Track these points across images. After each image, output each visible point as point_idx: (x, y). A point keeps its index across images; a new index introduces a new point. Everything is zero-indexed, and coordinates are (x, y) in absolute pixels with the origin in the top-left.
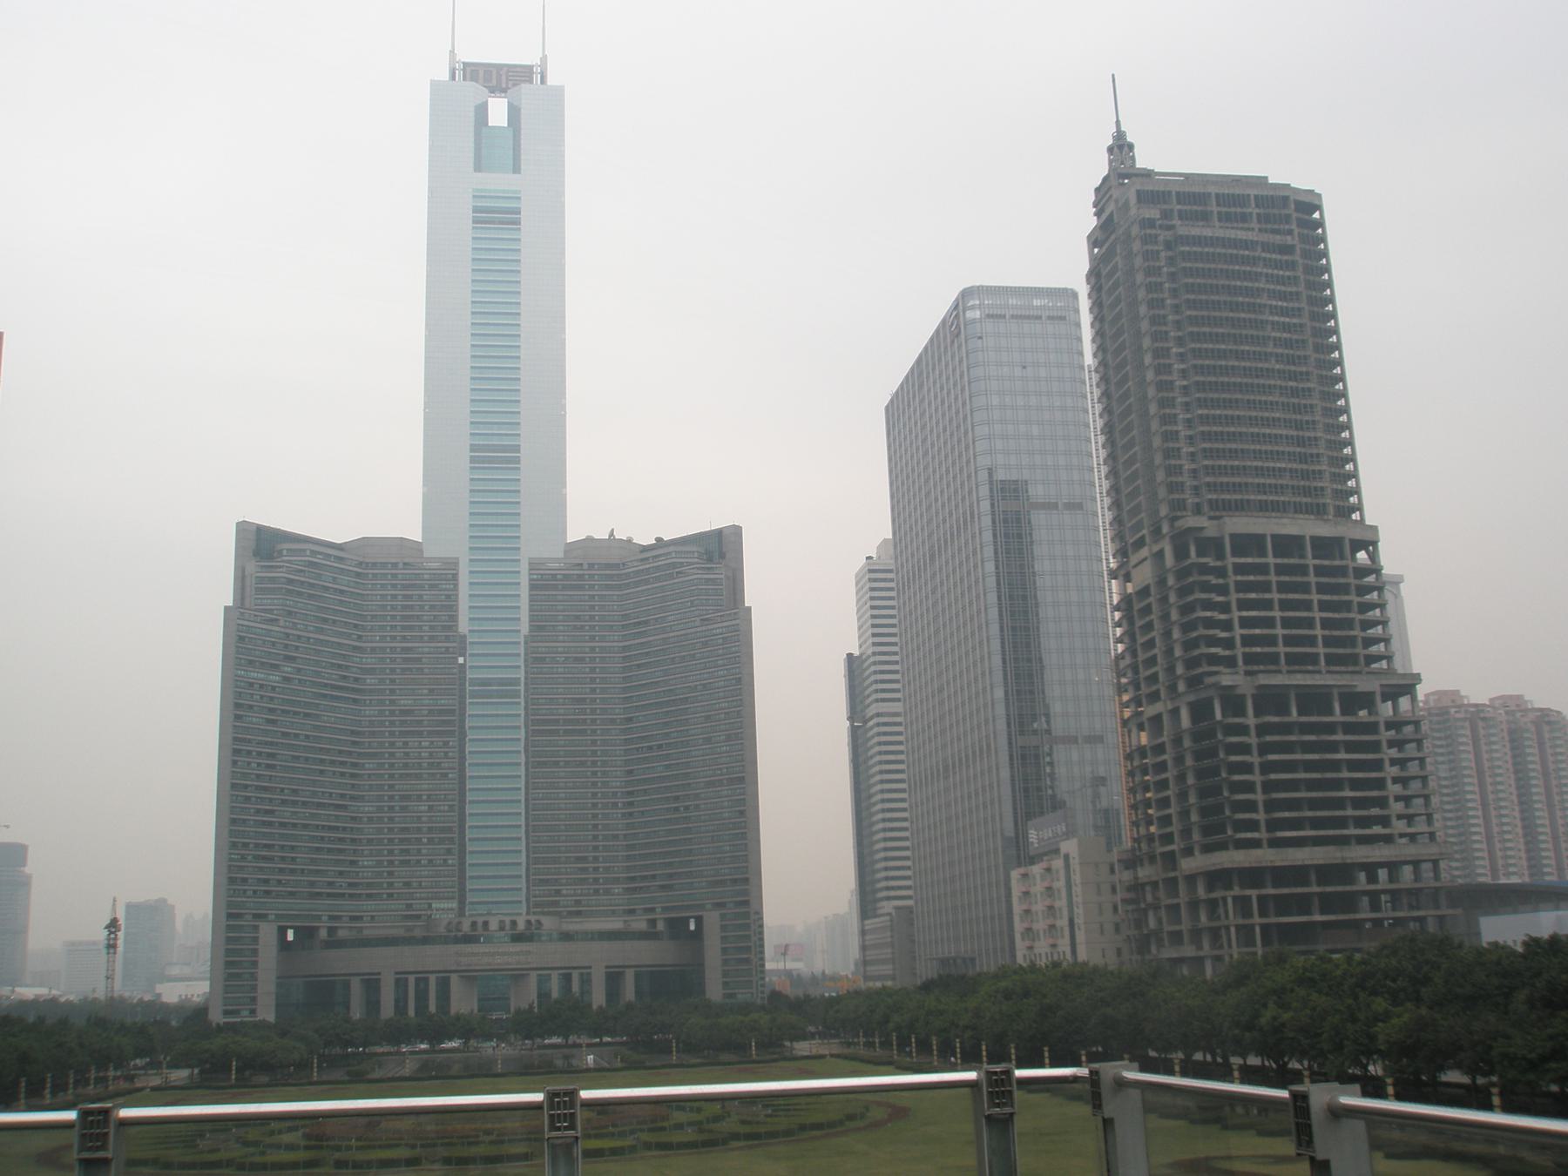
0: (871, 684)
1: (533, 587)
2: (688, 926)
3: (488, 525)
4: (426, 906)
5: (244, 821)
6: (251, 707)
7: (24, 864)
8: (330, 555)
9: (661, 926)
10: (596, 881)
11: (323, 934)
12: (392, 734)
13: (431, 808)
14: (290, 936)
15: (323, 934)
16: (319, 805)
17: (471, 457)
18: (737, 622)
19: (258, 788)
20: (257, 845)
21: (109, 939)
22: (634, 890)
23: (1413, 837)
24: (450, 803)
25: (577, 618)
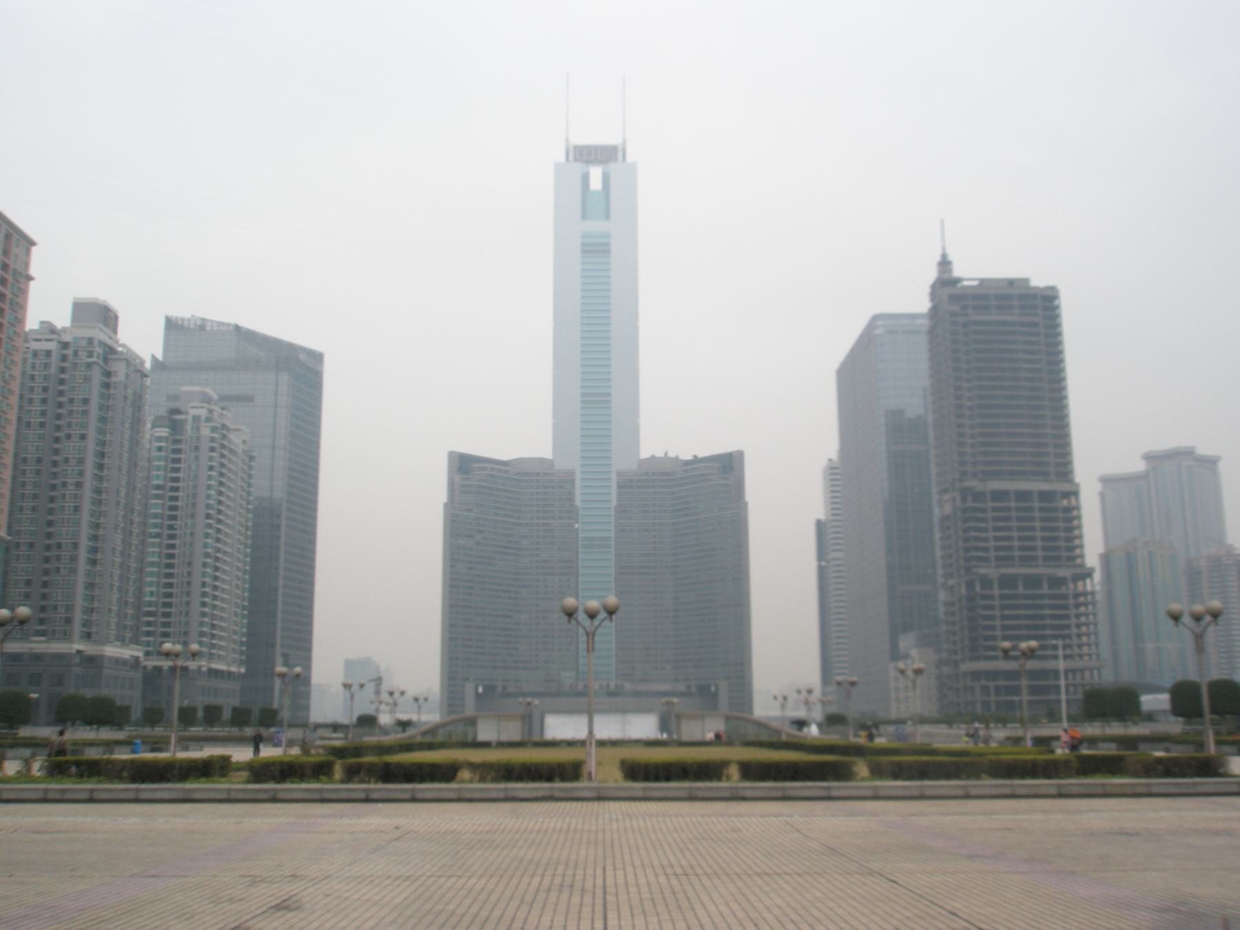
1: (620, 487)
9: (694, 689)
14: (480, 689)
15: (499, 689)
23: (1081, 656)
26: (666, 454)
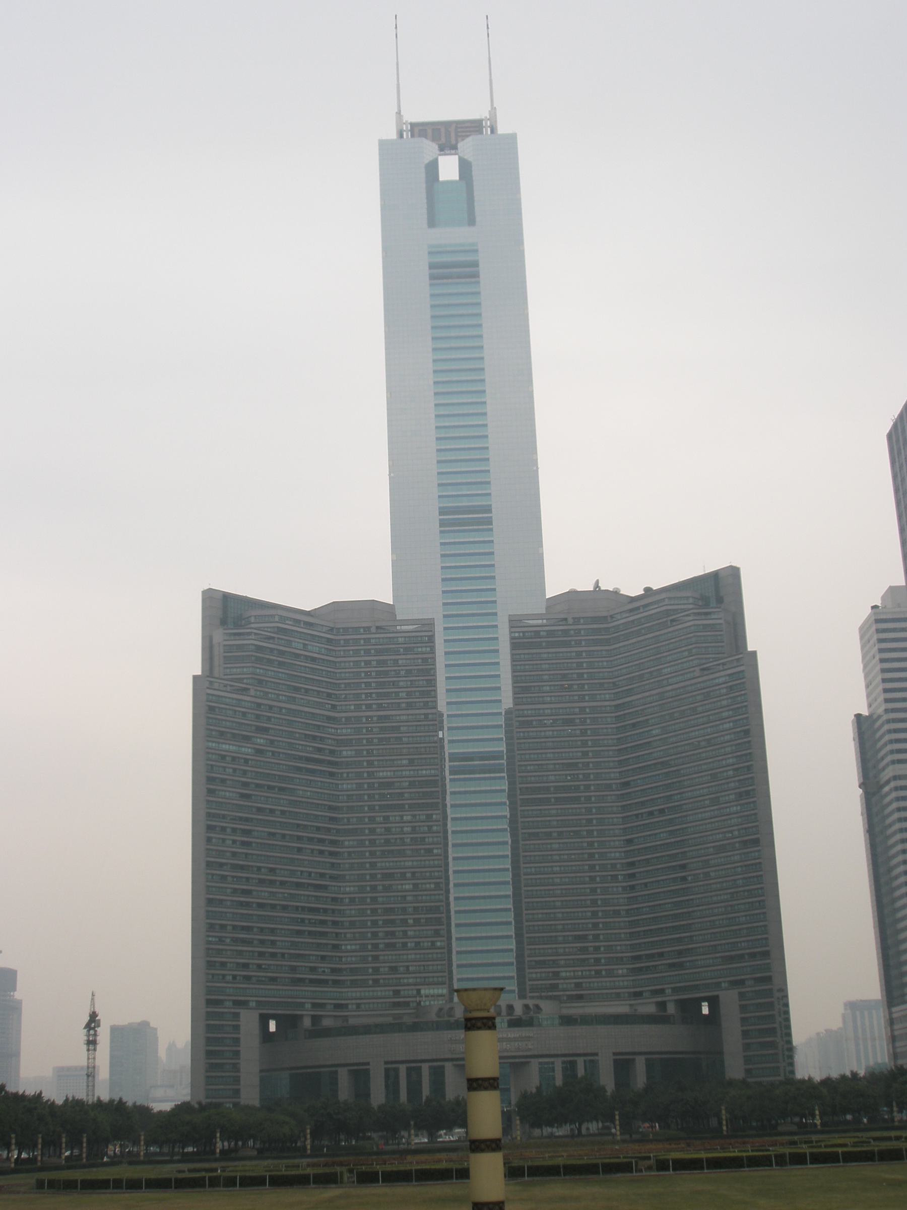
0: (885, 745)
4: (415, 992)
5: (221, 901)
6: (223, 781)
8: (300, 621)
9: (671, 1009)
11: (307, 1023)
12: (372, 809)
13: (415, 886)
14: (272, 1026)
15: (307, 1023)
16: (298, 885)
18: (742, 668)
19: (235, 867)
20: (234, 927)
21: (88, 1035)
25: (564, 677)
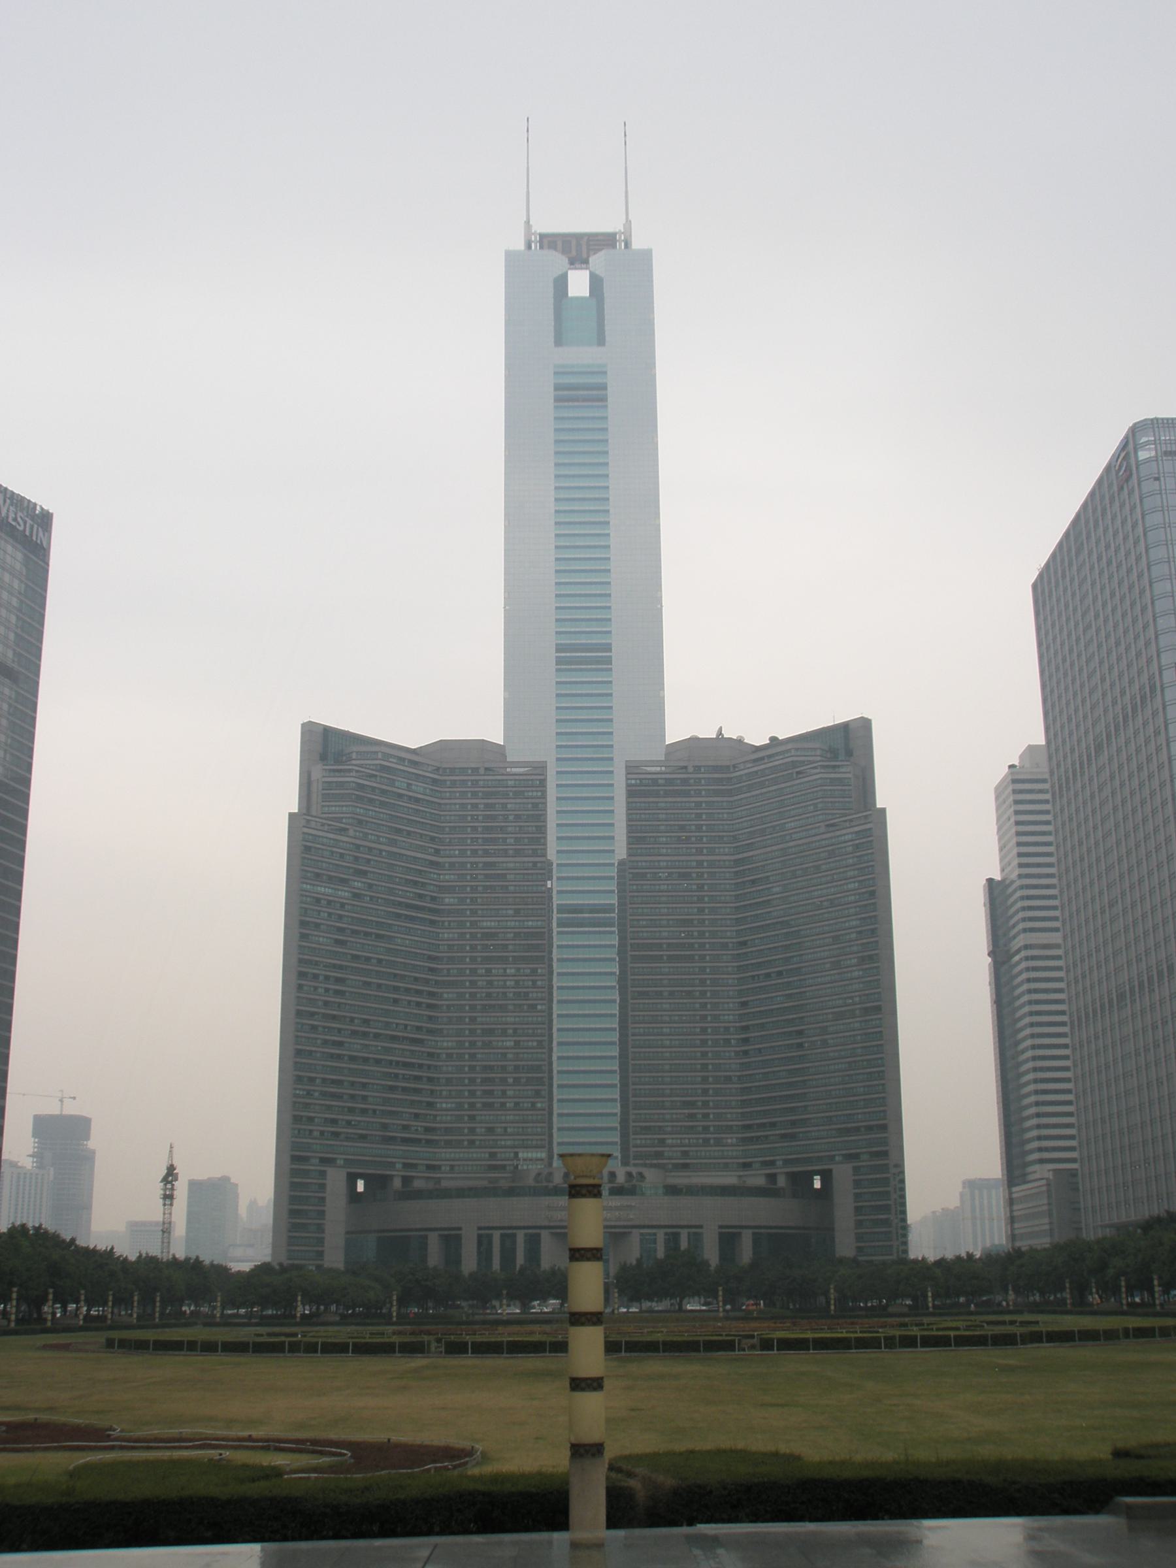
1: (631, 793)
2: (812, 1184)
3: (576, 733)
4: (512, 1155)
6: (317, 926)
7: (88, 1138)
9: (782, 1182)
10: (706, 1129)
11: (397, 1183)
12: (473, 960)
13: (517, 1043)
14: (360, 1186)
15: (397, 1183)
17: (557, 657)
20: (324, 1080)
22: (751, 1140)
24: (539, 1038)
26: (720, 732)
